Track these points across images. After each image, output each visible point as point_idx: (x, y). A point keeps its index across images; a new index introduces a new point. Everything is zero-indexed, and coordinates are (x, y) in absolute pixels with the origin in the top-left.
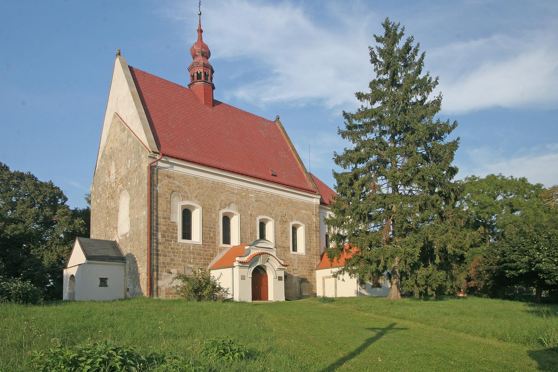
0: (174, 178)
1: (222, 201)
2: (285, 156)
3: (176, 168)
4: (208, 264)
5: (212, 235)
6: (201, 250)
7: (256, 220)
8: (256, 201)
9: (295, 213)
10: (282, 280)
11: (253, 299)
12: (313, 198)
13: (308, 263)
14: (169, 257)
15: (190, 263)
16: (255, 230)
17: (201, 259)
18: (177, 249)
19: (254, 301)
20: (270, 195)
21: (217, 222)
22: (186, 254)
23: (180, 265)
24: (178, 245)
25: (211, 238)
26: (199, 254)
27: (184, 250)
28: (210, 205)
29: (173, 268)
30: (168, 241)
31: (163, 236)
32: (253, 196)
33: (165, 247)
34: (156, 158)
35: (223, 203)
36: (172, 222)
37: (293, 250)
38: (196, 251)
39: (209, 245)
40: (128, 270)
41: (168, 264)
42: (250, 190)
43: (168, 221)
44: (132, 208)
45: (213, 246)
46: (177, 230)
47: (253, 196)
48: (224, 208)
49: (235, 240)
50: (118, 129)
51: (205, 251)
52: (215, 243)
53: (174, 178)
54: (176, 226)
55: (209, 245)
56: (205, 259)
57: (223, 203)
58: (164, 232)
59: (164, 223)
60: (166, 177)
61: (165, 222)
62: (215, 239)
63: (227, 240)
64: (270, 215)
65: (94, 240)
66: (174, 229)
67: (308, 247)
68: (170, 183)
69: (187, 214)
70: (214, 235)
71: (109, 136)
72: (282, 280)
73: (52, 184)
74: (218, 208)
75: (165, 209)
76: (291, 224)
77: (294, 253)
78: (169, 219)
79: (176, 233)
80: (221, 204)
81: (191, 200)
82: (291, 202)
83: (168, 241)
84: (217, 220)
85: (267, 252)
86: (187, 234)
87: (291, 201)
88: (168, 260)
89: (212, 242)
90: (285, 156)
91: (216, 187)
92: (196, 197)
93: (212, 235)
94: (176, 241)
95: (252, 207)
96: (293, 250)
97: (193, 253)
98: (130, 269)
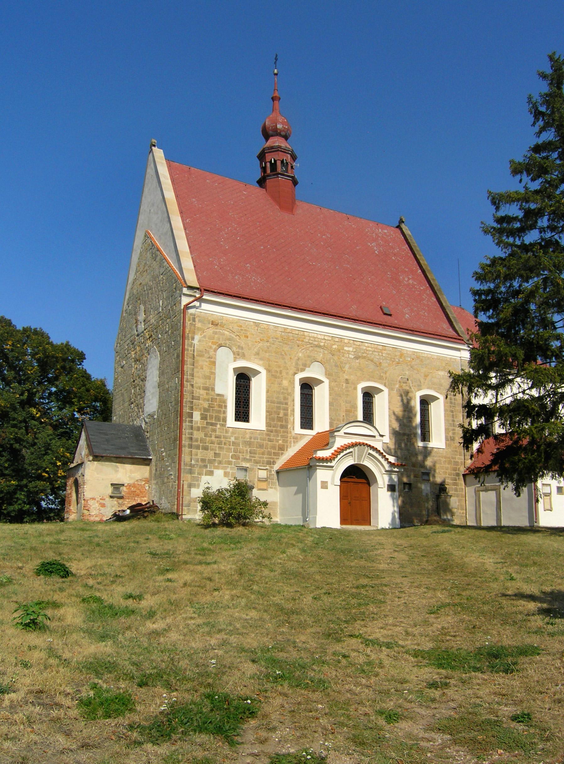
0: (222, 326)
1: (298, 359)
2: (411, 281)
3: (204, 306)
4: (274, 463)
5: (281, 415)
6: (264, 440)
7: (355, 389)
8: (357, 358)
9: (426, 376)
10: (322, 482)
11: (343, 521)
12: (459, 350)
13: (450, 463)
14: (212, 450)
15: (245, 460)
16: (355, 407)
17: (263, 454)
18: (225, 437)
19: (344, 526)
20: (380, 348)
21: (292, 394)
22: (239, 445)
23: (229, 463)
24: (227, 432)
25: (280, 419)
26: (261, 446)
27: (236, 438)
28: (279, 367)
29: (217, 468)
30: (212, 424)
31: (204, 417)
32: (351, 349)
33: (206, 435)
34: (195, 296)
35: (300, 363)
36: (218, 395)
37: (303, 426)
38: (252, 442)
39: (276, 431)
40: (154, 472)
41: (211, 461)
42: (346, 341)
43: (212, 393)
44: (162, 373)
45: (284, 432)
46: (226, 407)
47: (351, 349)
48: (303, 370)
49: (321, 423)
50: (149, 255)
51: (270, 440)
52: (286, 427)
53: (222, 326)
54: (225, 402)
55: (276, 431)
56: (269, 453)
57: (300, 363)
58: (206, 410)
59: (205, 396)
60: (210, 326)
61: (207, 394)
62: (287, 421)
63: (307, 421)
64: (380, 379)
65: (119, 425)
66: (220, 406)
67: (451, 434)
68: (215, 333)
69: (243, 380)
70: (286, 415)
71: (139, 265)
72: (322, 482)
73: (67, 345)
74: (291, 372)
75: (208, 374)
76: (361, 386)
77: (241, 425)
78: (213, 389)
79: (225, 412)
80: (297, 364)
81: (249, 360)
82: (418, 357)
83: (212, 424)
84: (290, 391)
85: (366, 442)
86: (243, 413)
87: (417, 356)
88: (210, 455)
89: (282, 426)
90: (411, 281)
91: (290, 338)
92: (257, 354)
93: (281, 415)
94: (224, 425)
95: (350, 368)
96: (303, 426)
97: (249, 444)
98: (156, 470)
